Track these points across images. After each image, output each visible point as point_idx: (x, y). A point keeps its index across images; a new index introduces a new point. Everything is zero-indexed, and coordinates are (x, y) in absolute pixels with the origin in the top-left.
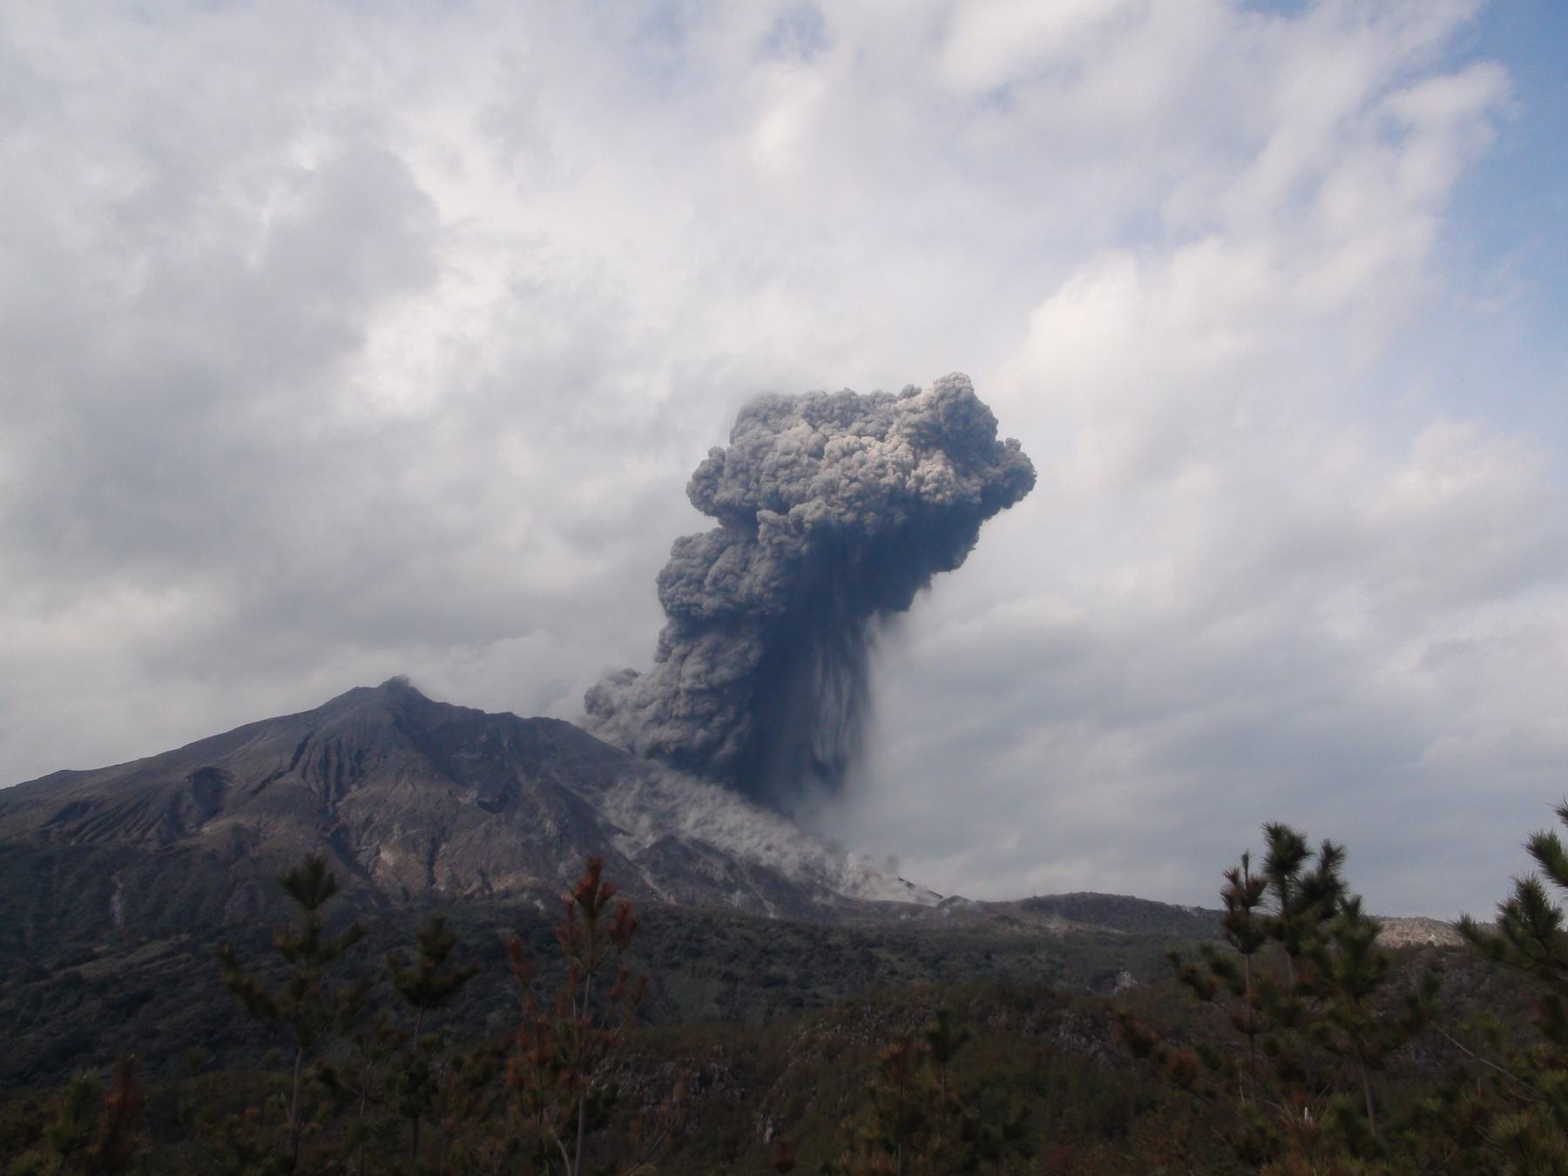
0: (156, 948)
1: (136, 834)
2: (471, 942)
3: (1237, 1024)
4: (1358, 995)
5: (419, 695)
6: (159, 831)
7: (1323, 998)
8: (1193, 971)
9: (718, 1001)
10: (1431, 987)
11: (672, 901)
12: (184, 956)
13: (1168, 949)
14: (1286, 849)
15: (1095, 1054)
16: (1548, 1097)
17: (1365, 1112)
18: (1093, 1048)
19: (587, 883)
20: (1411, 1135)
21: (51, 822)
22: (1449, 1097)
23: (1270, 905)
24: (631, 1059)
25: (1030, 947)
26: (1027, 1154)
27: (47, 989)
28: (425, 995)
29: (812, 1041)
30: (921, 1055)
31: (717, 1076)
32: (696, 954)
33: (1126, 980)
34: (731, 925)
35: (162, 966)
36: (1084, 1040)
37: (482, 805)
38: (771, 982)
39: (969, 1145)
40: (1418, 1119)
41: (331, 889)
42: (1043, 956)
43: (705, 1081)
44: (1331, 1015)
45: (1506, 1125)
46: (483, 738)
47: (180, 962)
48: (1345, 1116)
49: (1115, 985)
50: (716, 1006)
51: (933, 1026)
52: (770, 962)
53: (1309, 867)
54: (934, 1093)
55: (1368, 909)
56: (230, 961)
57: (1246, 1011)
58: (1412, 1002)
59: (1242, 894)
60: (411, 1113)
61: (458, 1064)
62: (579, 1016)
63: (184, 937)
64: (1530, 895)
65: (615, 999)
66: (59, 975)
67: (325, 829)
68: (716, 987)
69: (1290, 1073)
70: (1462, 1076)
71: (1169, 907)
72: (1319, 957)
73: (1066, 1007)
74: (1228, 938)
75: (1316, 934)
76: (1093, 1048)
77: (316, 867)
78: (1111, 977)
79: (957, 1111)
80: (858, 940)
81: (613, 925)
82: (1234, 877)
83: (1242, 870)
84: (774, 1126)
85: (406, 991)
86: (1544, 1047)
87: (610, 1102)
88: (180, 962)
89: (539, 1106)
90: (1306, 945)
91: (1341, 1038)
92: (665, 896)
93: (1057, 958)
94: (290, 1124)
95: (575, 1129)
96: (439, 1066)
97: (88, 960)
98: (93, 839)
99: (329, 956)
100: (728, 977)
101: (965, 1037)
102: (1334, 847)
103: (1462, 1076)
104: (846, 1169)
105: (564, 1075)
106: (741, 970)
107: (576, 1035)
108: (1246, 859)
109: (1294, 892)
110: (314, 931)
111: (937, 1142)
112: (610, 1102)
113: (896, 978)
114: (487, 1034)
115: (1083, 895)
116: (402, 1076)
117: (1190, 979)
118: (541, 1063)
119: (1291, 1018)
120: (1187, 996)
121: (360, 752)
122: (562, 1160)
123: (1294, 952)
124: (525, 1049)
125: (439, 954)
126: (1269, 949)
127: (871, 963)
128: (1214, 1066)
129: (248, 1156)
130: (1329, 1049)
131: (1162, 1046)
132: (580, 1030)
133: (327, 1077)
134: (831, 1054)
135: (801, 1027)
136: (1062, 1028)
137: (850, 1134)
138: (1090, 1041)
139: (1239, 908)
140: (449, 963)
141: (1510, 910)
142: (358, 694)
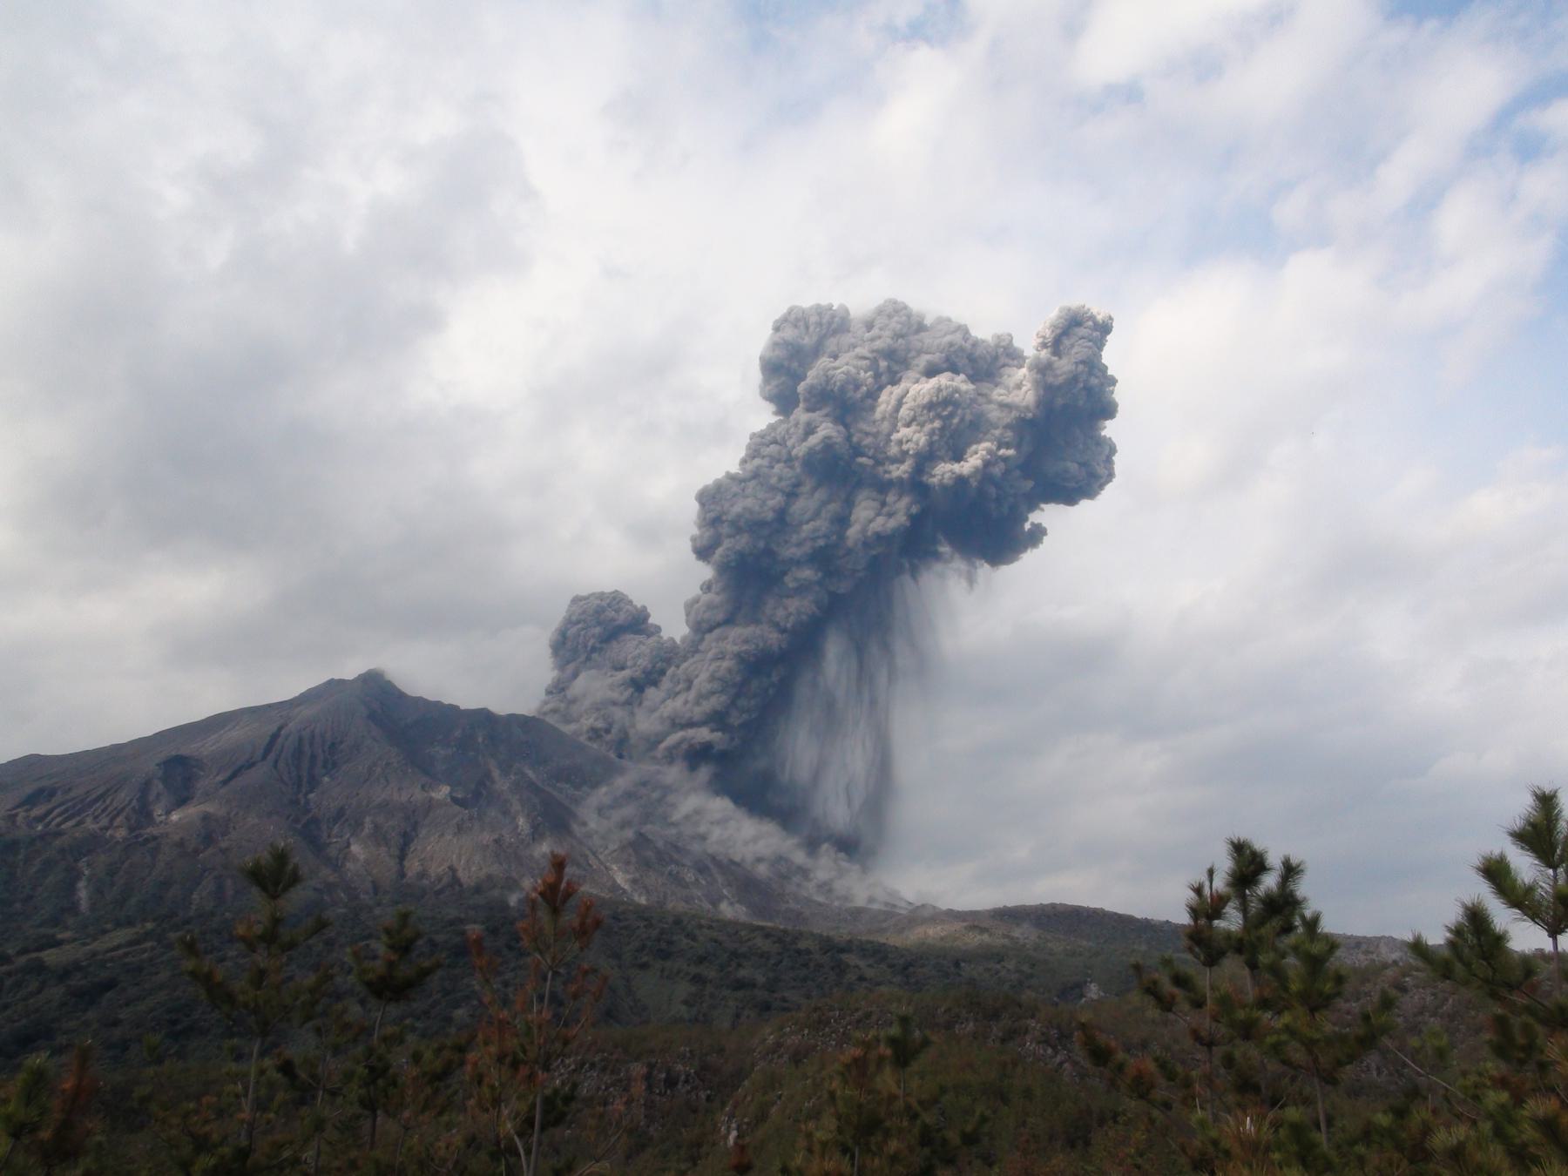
0: (121, 936)
1: (104, 822)
2: (440, 938)
3: (1196, 1035)
4: (1313, 1010)
5: (394, 687)
6: (127, 818)
7: (1279, 1013)
8: (1155, 983)
9: (686, 1002)
10: (1387, 1004)
11: (643, 901)
12: (149, 944)
13: (1132, 960)
14: (1248, 863)
15: (1061, 1063)
16: (1490, 1116)
17: (1318, 1127)
18: (1059, 1059)
19: (551, 879)
20: (1360, 1149)
21: (18, 806)
22: (1401, 1113)
23: (1232, 921)
24: (597, 1059)
25: (998, 956)
26: (989, 1161)
27: (9, 974)
28: (387, 988)
29: (778, 1045)
30: (881, 1060)
31: (683, 1078)
32: (665, 955)
33: (1093, 991)
34: (701, 927)
35: (126, 955)
36: (1050, 1051)
37: (455, 800)
38: (740, 985)
39: (927, 1151)
40: (1368, 1134)
41: (295, 879)
42: (1011, 965)
43: (671, 1082)
44: (1287, 1029)
45: (1441, 1139)
46: (458, 733)
47: (145, 951)
48: (1297, 1130)
49: (1082, 996)
50: (684, 1008)
51: (895, 1031)
52: (739, 965)
53: (1269, 882)
54: (892, 1098)
55: (1328, 926)
56: (191, 948)
57: (1206, 1024)
58: (1366, 1018)
59: (1207, 908)
60: (370, 1105)
61: (417, 1058)
62: (540, 1012)
63: (149, 926)
64: (1476, 918)
65: (575, 996)
66: (22, 960)
67: (297, 821)
68: (684, 989)
69: (1245, 1085)
70: (1415, 1093)
71: (1138, 920)
72: (1276, 971)
73: (1033, 1017)
74: (1191, 950)
75: (1275, 950)
76: (1059, 1059)
77: (281, 857)
78: (1073, 990)
79: (915, 1116)
80: (830, 946)
81: (576, 924)
82: (1198, 890)
83: (1207, 884)
84: (738, 1129)
85: (369, 984)
86: (1494, 1067)
87: (569, 1099)
88: (145, 951)
89: (497, 1102)
90: (1264, 959)
91: (1298, 1055)
92: (636, 898)
93: (1026, 968)
94: (246, 1114)
95: (532, 1126)
96: (400, 1060)
97: (52, 946)
98: (59, 825)
99: (292, 945)
100: (697, 979)
101: (926, 1043)
102: (1294, 861)
103: (1415, 1093)
104: (800, 1171)
105: (524, 1071)
106: (710, 972)
107: (535, 1031)
108: (1211, 873)
109: (1254, 906)
110: (276, 921)
111: (893, 1145)
112: (569, 1099)
113: (864, 984)
114: (453, 1030)
115: (1053, 906)
116: (361, 1070)
117: (1152, 990)
118: (501, 1058)
119: (1248, 1031)
120: (1153, 1013)
121: (333, 744)
122: (519, 1155)
123: (1253, 966)
124: (486, 1044)
125: (404, 948)
126: (1232, 966)
127: (840, 969)
128: (1171, 1076)
129: (202, 1144)
130: (1284, 1062)
131: (1120, 1056)
132: (540, 1027)
133: (287, 1068)
134: (797, 1058)
135: (768, 1030)
136: (1028, 1038)
137: (809, 1135)
138: (1056, 1052)
139: (1202, 922)
140: (417, 959)
141: (1458, 932)
142: (333, 685)
